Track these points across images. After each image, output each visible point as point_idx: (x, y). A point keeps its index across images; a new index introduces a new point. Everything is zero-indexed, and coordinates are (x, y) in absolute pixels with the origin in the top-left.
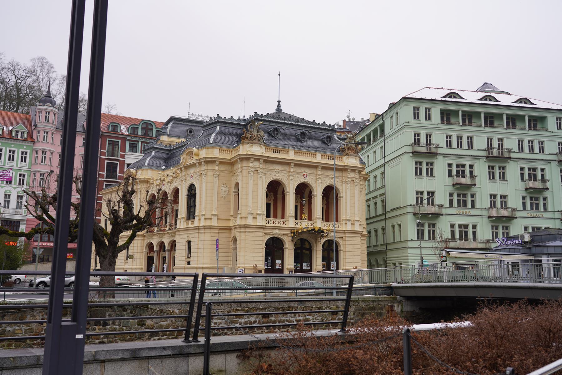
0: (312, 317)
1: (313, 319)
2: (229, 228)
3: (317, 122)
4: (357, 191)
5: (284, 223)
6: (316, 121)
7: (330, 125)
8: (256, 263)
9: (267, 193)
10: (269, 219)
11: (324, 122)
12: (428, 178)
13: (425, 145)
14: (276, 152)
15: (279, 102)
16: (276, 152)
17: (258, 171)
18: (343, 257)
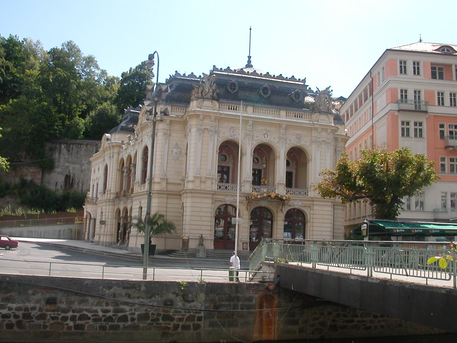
0: (130, 308)
1: (131, 310)
2: (311, 199)
3: (285, 76)
4: (329, 153)
5: (300, 193)
6: (270, 74)
7: (274, 76)
8: (202, 233)
9: (287, 161)
10: (221, 184)
11: (281, 75)
12: (416, 139)
13: (413, 103)
14: (231, 109)
15: (249, 57)
16: (231, 109)
17: (326, 142)
18: (310, 229)
